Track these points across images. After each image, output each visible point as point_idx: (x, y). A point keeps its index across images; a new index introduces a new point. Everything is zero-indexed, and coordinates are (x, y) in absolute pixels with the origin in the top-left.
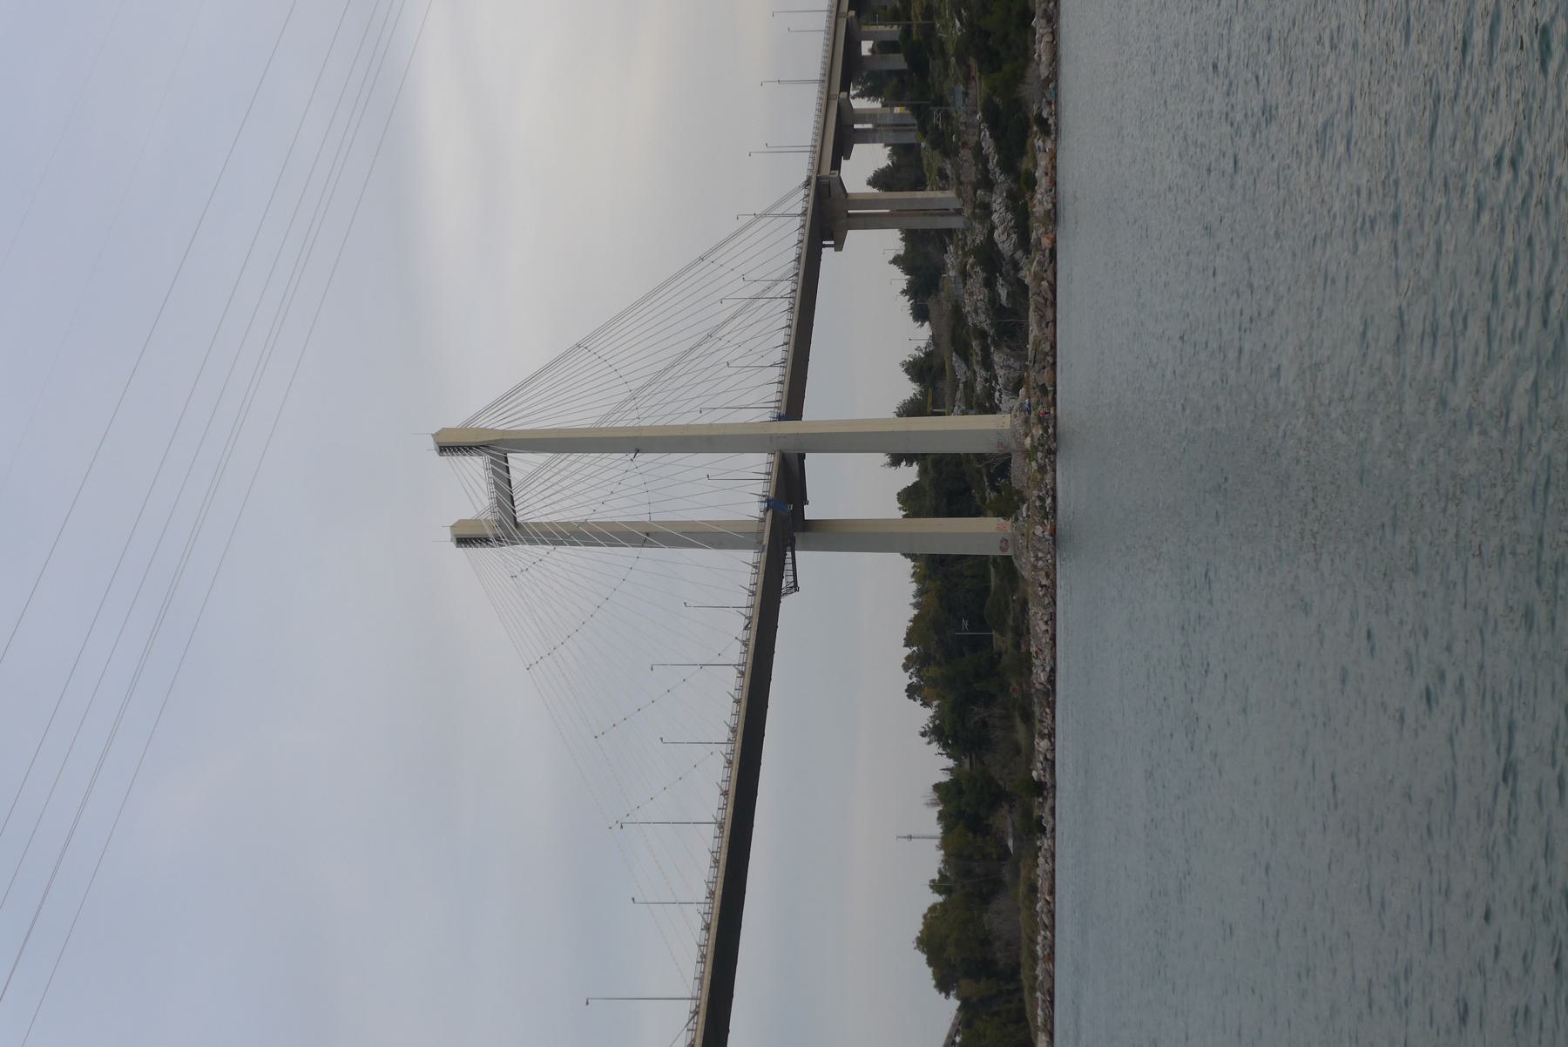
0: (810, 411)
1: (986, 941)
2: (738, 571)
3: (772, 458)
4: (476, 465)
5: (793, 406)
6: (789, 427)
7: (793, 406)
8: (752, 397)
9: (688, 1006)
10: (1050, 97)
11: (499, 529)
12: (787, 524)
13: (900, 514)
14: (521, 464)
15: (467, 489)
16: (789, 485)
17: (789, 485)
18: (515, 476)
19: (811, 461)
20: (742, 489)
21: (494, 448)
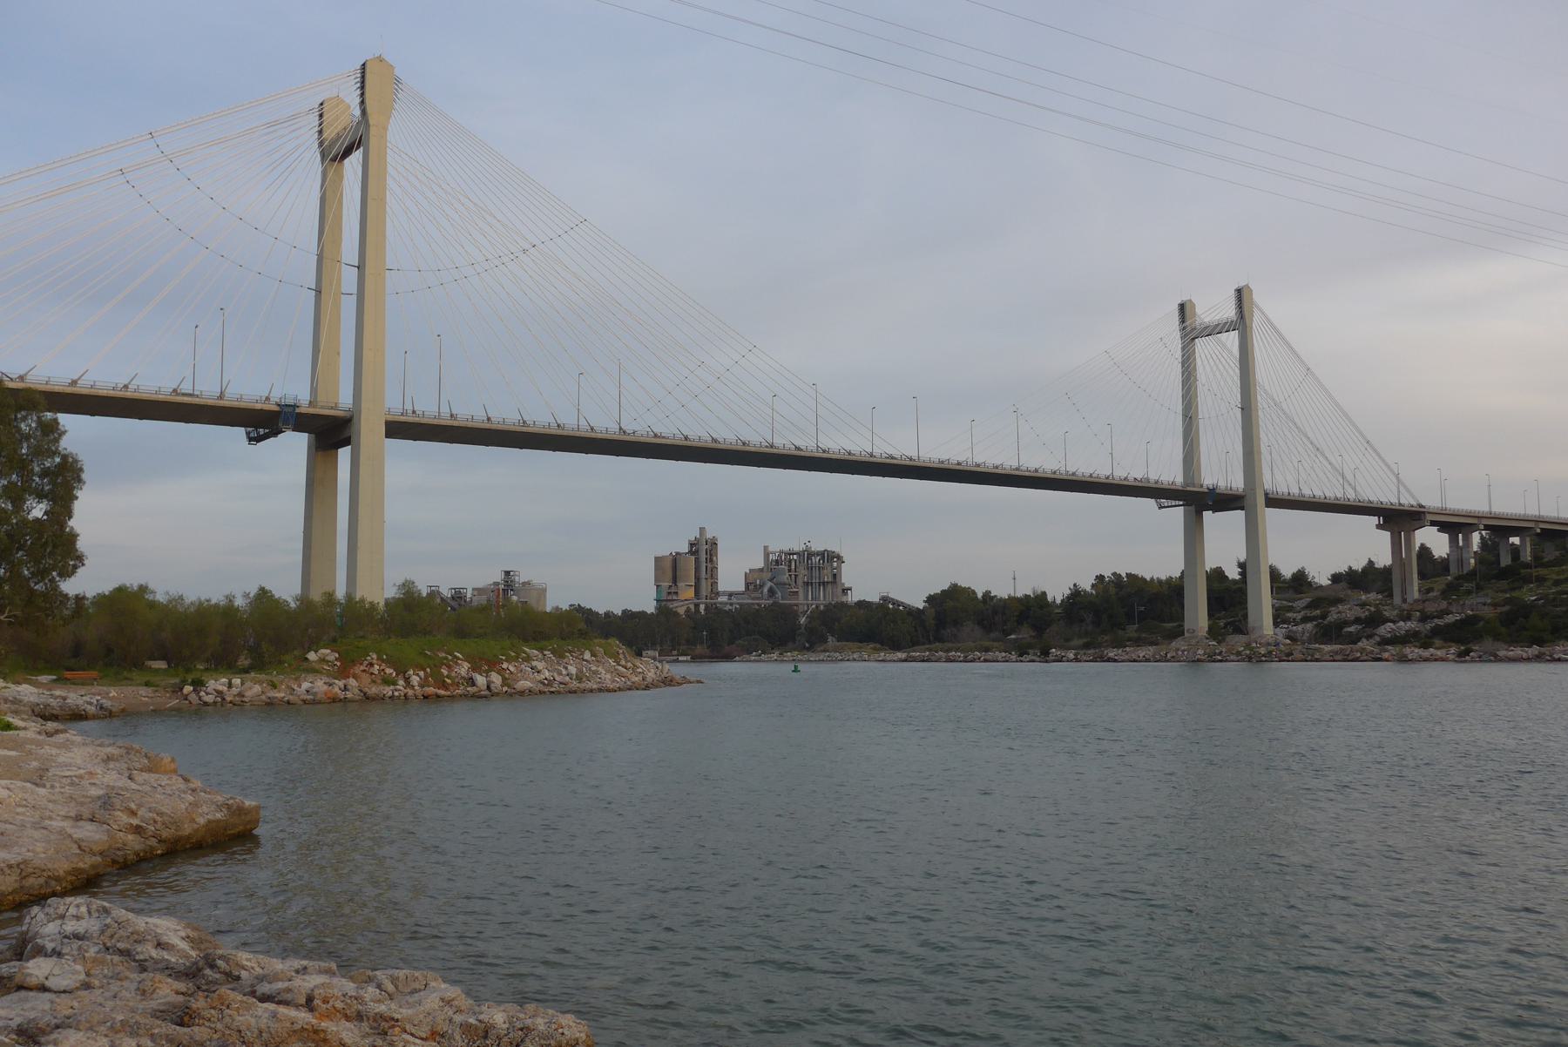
2: (1170, 473)
4: (1230, 312)
5: (1274, 502)
6: (1261, 500)
7: (1274, 502)
14: (1232, 339)
15: (1215, 306)
16: (1224, 501)
17: (1224, 501)
20: (1222, 472)
21: (1241, 322)
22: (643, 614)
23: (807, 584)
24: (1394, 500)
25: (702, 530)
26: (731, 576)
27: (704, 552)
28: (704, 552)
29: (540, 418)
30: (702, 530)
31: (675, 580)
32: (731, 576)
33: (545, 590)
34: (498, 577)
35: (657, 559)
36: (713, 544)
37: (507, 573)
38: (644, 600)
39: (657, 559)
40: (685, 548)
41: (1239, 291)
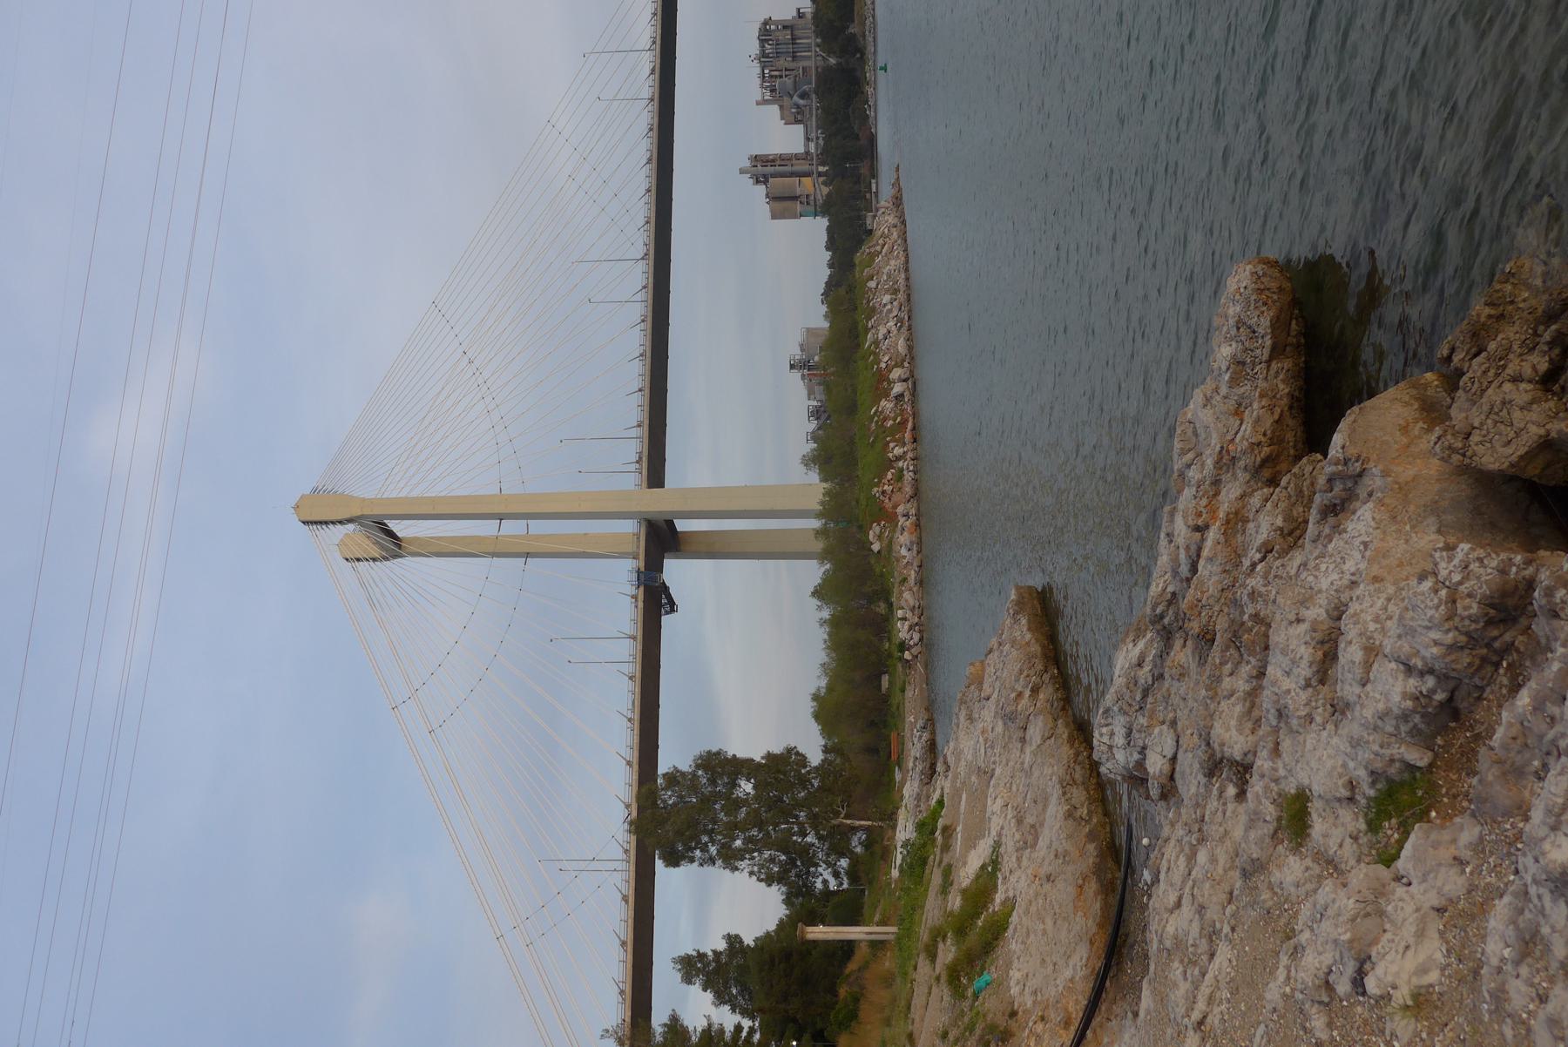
10: (882, 608)
22: (830, 230)
23: (794, 57)
24: (646, 171)
25: (742, 171)
26: (788, 139)
27: (765, 169)
28: (765, 169)
30: (742, 171)
31: (794, 198)
34: (797, 375)
35: (774, 217)
36: (756, 159)
37: (792, 367)
39: (774, 217)
40: (762, 189)
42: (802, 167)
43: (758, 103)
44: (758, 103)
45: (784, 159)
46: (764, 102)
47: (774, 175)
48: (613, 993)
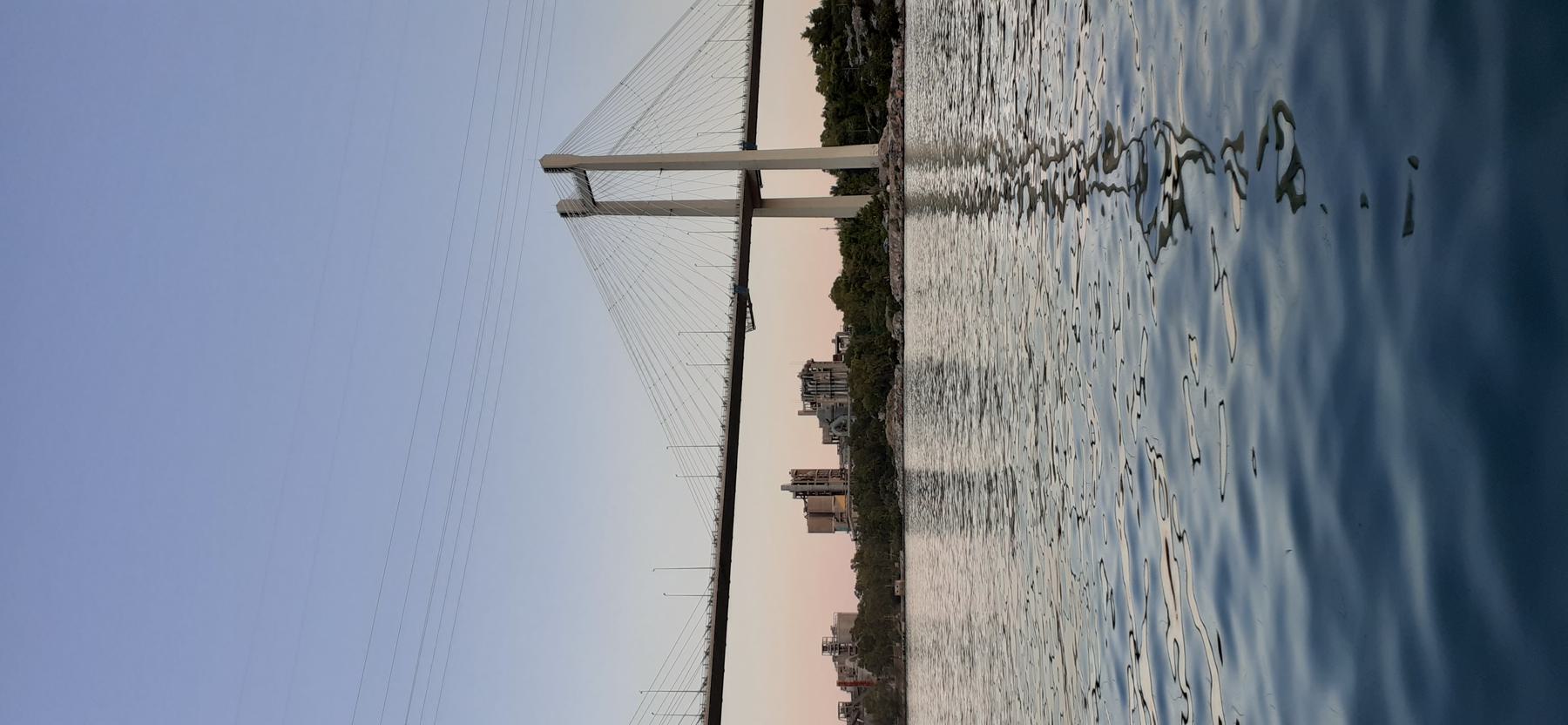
0: (762, 143)
1: (874, 646)
2: (729, 226)
3: (735, 219)
4: (568, 179)
5: (750, 143)
6: (749, 156)
7: (750, 143)
8: (731, 142)
9: (710, 573)
10: (853, 249)
11: (586, 206)
12: (752, 202)
13: (820, 144)
14: (595, 177)
15: (567, 185)
16: (752, 184)
17: (752, 184)
18: (592, 183)
19: (763, 172)
20: (727, 186)
21: (579, 169)
22: (860, 562)
23: (832, 395)
24: (742, 116)
25: (784, 488)
26: (828, 458)
27: (805, 484)
28: (805, 484)
29: (703, 615)
30: (784, 488)
31: (831, 514)
32: (828, 458)
33: (840, 615)
34: (828, 657)
35: (810, 531)
36: (796, 473)
37: (824, 649)
38: (843, 545)
39: (810, 531)
40: (800, 503)
41: (547, 170)
42: (836, 484)
43: (800, 413)
44: (800, 413)
45: (823, 475)
46: (804, 413)
47: (811, 493)
48: (710, 540)
